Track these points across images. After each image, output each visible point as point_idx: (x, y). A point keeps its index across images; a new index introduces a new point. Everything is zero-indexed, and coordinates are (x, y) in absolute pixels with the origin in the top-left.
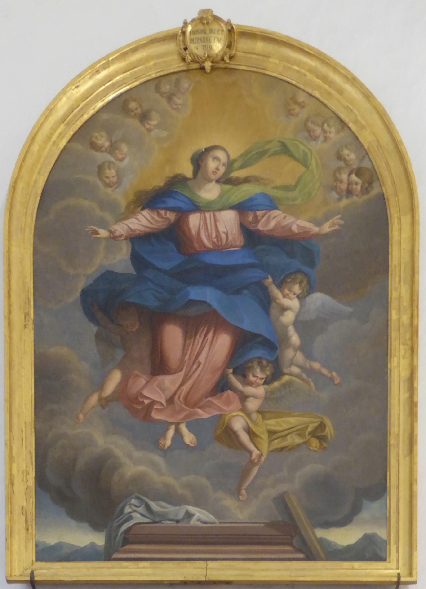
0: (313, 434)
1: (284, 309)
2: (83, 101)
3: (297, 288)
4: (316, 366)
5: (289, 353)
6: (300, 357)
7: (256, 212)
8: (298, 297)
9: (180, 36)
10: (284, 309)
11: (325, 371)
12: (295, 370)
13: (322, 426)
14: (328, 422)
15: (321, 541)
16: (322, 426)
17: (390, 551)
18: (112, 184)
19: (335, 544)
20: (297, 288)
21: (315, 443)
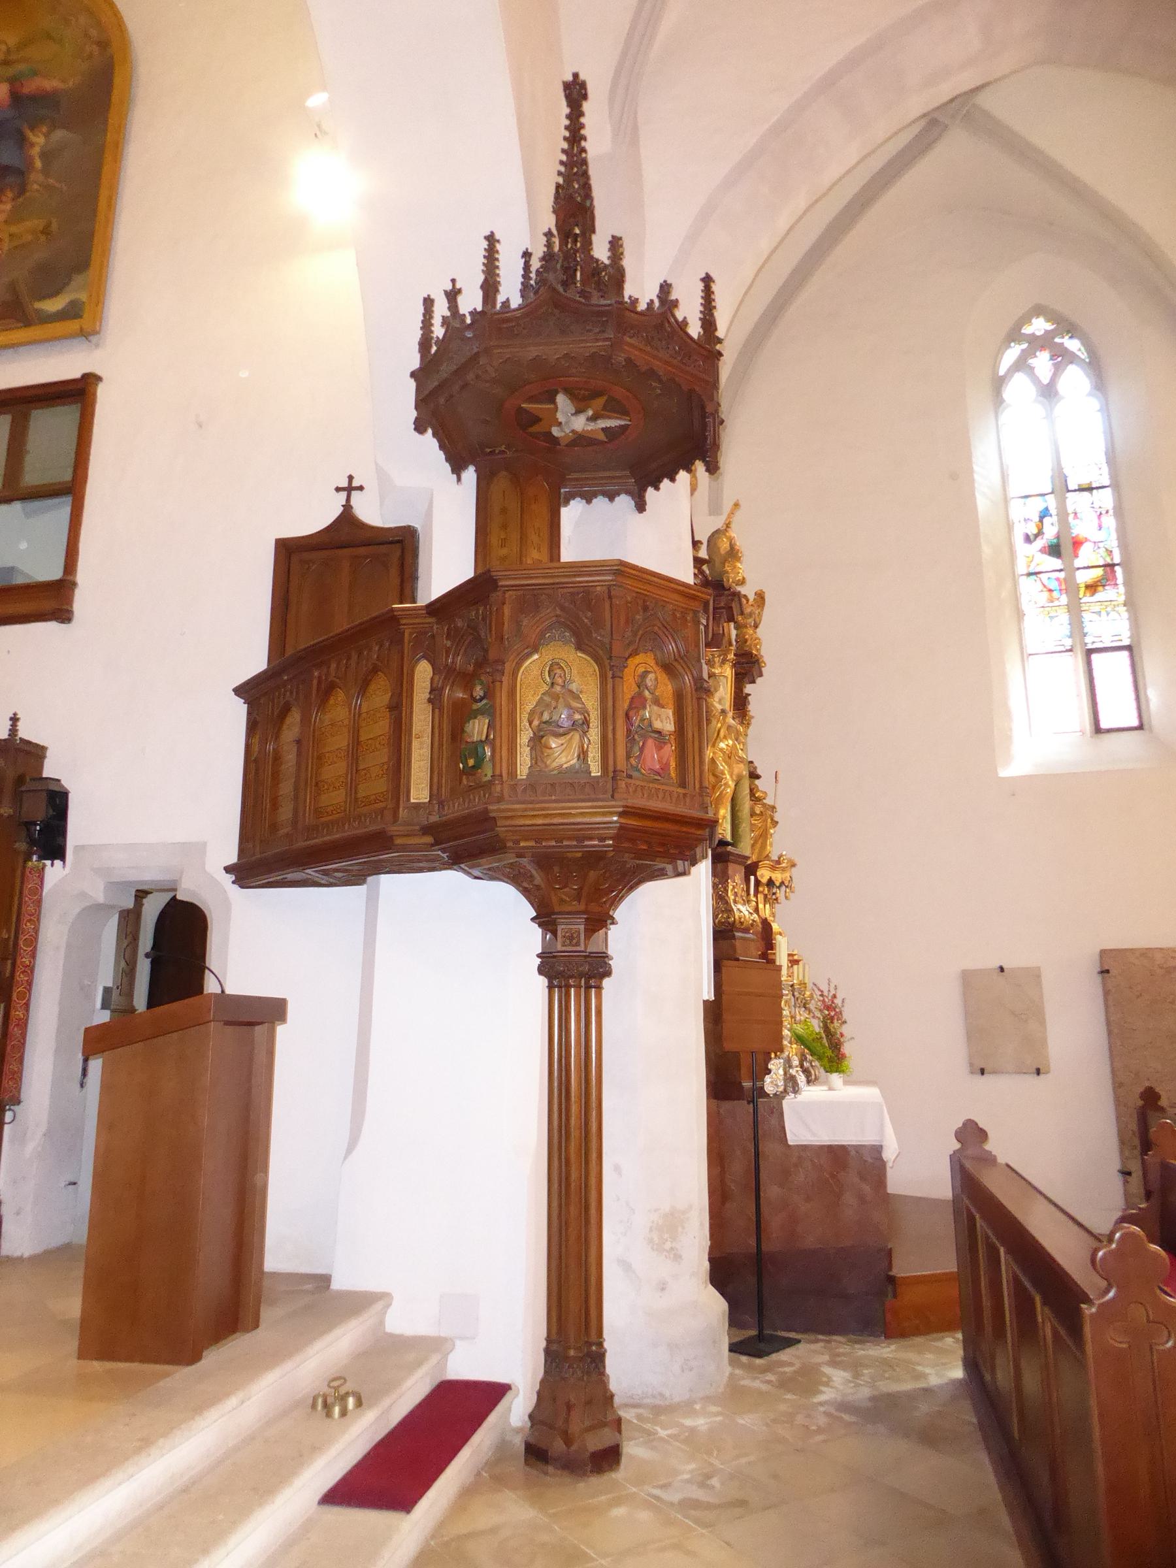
0: (42, 232)
1: (32, 145)
2: (1101, 1415)
3: (44, 129)
4: (51, 181)
5: (33, 176)
6: (41, 178)
7: (22, 485)
8: (44, 134)
9: (724, 817)
10: (32, 145)
11: (57, 185)
12: (35, 186)
13: (49, 225)
14: (54, 221)
15: (38, 311)
16: (49, 225)
17: (91, 423)
18: (1055, 541)
19: (47, 311)
20: (44, 129)
21: (43, 238)
